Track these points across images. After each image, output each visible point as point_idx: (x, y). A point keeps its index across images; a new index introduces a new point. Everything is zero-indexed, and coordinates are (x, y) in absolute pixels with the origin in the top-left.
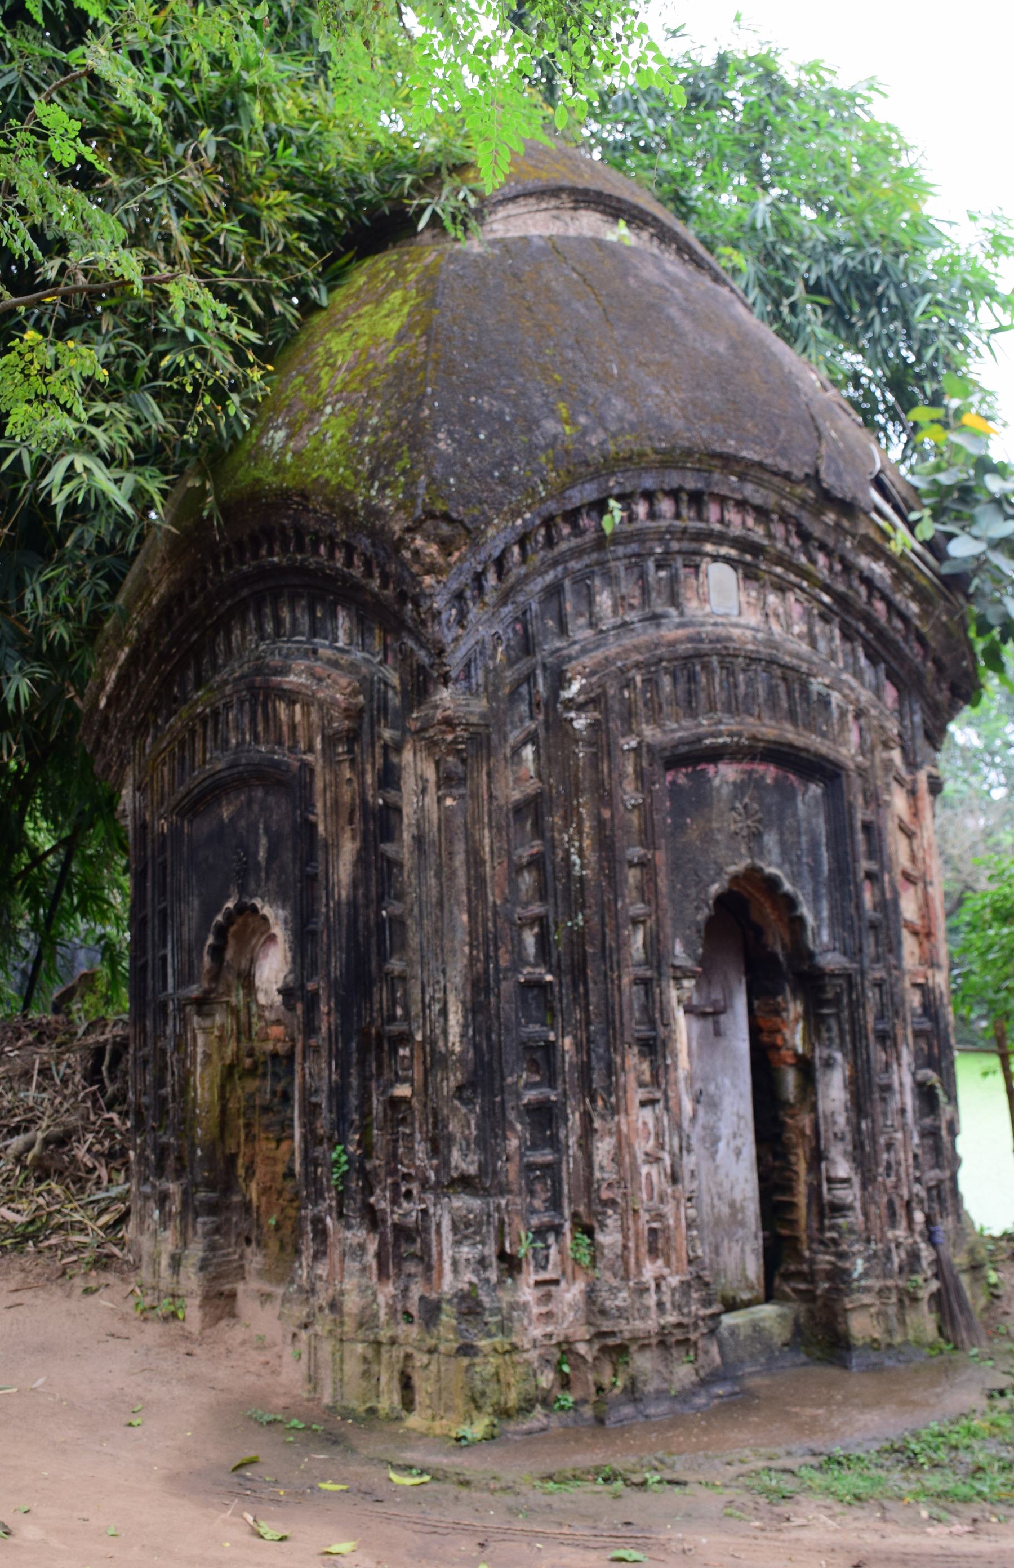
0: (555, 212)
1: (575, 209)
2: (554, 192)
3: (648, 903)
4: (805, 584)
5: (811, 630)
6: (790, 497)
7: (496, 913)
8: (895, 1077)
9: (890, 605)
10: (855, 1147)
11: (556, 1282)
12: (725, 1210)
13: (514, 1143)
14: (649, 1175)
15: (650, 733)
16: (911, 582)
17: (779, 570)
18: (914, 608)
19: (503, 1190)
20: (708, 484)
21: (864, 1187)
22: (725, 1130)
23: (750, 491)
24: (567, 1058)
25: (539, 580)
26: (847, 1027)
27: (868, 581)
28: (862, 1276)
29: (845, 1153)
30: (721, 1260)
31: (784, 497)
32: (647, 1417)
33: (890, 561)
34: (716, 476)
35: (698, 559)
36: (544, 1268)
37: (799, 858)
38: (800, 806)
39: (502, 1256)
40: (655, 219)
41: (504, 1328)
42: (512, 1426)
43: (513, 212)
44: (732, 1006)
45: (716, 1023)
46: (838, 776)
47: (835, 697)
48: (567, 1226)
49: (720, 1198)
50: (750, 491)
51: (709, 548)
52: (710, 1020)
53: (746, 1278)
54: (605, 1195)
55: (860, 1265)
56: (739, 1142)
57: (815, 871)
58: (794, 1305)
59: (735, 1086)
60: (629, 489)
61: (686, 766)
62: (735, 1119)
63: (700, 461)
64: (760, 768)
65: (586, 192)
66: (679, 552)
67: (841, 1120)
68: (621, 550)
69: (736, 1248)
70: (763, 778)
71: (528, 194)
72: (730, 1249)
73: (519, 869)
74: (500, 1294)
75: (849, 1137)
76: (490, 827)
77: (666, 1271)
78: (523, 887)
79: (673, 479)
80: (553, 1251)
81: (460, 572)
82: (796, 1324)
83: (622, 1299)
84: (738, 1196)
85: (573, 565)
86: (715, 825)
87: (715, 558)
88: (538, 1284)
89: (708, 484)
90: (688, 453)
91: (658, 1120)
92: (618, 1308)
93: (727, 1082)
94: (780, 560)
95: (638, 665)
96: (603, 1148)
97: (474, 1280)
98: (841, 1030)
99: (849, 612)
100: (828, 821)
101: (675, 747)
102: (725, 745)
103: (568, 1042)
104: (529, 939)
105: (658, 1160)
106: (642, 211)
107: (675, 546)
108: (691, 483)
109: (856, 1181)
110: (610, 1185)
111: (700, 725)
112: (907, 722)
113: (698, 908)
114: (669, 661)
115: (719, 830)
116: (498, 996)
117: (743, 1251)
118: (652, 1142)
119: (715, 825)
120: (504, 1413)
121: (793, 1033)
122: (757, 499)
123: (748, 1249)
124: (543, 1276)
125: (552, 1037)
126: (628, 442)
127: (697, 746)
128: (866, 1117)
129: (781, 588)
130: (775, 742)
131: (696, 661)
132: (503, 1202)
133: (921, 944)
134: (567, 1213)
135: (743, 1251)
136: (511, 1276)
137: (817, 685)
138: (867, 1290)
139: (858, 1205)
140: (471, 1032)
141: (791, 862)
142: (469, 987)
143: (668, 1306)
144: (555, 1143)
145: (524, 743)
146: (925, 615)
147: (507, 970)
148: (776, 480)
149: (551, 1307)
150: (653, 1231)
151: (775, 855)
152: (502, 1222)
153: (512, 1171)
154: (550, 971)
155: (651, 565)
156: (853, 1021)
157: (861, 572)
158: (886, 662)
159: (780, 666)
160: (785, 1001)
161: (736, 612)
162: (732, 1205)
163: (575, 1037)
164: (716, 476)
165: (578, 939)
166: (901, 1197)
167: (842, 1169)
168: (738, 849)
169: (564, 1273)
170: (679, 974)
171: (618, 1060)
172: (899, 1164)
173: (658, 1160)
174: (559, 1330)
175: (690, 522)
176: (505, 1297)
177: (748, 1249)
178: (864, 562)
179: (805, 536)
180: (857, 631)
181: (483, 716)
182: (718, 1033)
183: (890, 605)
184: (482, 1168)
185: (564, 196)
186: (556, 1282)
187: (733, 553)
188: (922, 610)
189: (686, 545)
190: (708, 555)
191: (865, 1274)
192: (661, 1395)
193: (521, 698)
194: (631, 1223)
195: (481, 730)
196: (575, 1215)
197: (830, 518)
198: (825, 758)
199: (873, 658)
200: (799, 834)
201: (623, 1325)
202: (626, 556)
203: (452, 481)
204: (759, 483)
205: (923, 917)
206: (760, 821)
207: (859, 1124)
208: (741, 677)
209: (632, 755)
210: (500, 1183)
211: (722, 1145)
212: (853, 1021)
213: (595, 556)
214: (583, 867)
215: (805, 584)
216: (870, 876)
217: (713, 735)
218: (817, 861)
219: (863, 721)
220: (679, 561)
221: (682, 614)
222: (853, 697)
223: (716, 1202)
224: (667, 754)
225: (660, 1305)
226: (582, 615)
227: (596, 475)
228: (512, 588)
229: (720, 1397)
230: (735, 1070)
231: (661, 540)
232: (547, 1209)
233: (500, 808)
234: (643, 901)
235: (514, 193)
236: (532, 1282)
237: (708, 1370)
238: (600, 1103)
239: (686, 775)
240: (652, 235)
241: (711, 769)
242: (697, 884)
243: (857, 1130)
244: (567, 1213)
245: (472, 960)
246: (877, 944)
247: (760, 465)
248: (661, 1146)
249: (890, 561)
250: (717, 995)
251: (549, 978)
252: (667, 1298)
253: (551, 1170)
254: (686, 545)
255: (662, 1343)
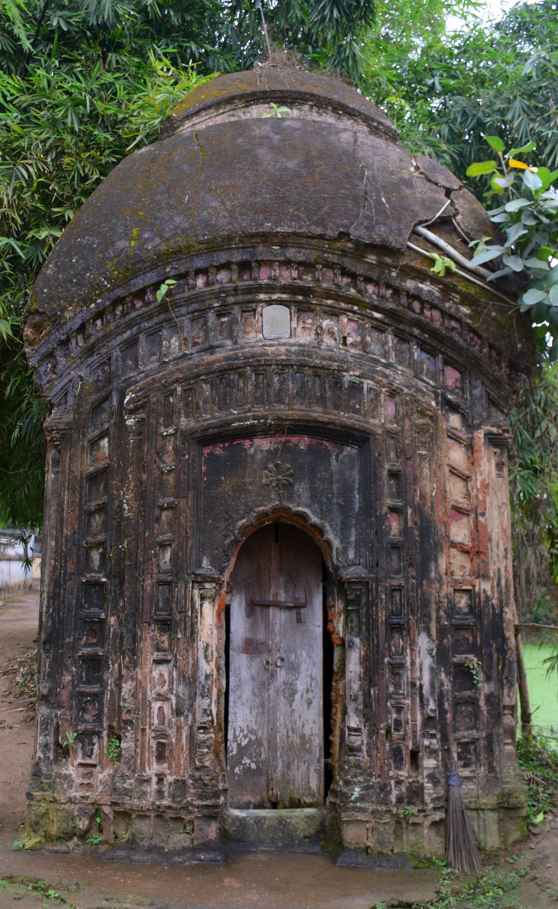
0: (231, 113)
1: (247, 106)
2: (229, 100)
3: (174, 533)
4: (356, 308)
5: (363, 339)
6: (331, 250)
7: (67, 541)
8: (408, 659)
9: (443, 313)
10: (365, 706)
11: (94, 766)
12: (297, 740)
13: (67, 678)
14: (160, 708)
15: (184, 423)
16: (457, 293)
17: (329, 302)
18: (465, 310)
19: (60, 707)
20: (253, 256)
21: (370, 736)
22: (301, 686)
23: (291, 253)
24: (112, 630)
25: (120, 337)
26: (364, 620)
27: (415, 296)
28: (357, 801)
29: (356, 710)
30: (291, 773)
31: (326, 252)
32: (131, 861)
33: (434, 279)
34: (260, 248)
35: (254, 305)
36: (90, 756)
37: (329, 500)
38: (334, 462)
39: (57, 744)
40: (312, 95)
41: (51, 787)
42: (49, 846)
43: (195, 122)
44: (311, 603)
45: (299, 614)
46: (368, 439)
47: (367, 383)
48: (105, 733)
49: (293, 731)
50: (291, 253)
51: (262, 296)
52: (294, 611)
53: (310, 788)
54: (125, 717)
55: (357, 791)
56: (311, 695)
57: (345, 509)
58: (325, 812)
59: (309, 656)
60: (183, 270)
61: (221, 442)
62: (309, 679)
63: (241, 241)
64: (294, 440)
65: (254, 94)
66: (235, 303)
67: (356, 686)
68: (183, 310)
69: (303, 768)
70: (297, 445)
71: (204, 109)
72: (298, 767)
73: (91, 514)
74: (54, 767)
75: (361, 699)
76: (68, 489)
77: (168, 772)
78: (95, 525)
79: (223, 257)
80: (96, 747)
81: (47, 342)
82: (322, 824)
83: (129, 783)
84: (307, 732)
85: (146, 324)
86: (247, 480)
87: (270, 302)
88: (81, 765)
89: (253, 256)
90: (229, 239)
91: (170, 673)
92: (125, 789)
93: (304, 654)
94: (328, 295)
95: (177, 381)
96: (127, 687)
97: (42, 756)
98: (360, 622)
99: (401, 322)
100: (360, 472)
101: (206, 429)
102: (253, 425)
103: (112, 620)
104: (96, 556)
105: (167, 699)
106: (301, 93)
107: (231, 300)
108: (237, 257)
109: (365, 731)
110: (129, 711)
111: (231, 414)
112: (467, 395)
113: (226, 536)
114: (206, 374)
115: (250, 483)
116: (65, 590)
117: (308, 769)
118: (166, 687)
119: (247, 480)
120: (48, 838)
121: (338, 623)
122: (300, 257)
123: (312, 769)
124: (88, 761)
125: (103, 616)
126: (181, 241)
127: (227, 428)
128: (374, 686)
129: (334, 313)
130: (299, 420)
131: (232, 372)
132: (59, 713)
133: (472, 560)
134: (105, 725)
135: (308, 769)
136: (65, 758)
137: (348, 377)
138: (363, 810)
139: (364, 748)
140: (51, 610)
141: (321, 504)
142: (52, 584)
143: (166, 794)
144: (101, 681)
145: (101, 437)
146: (475, 315)
147: (72, 574)
148: (314, 242)
149: (91, 781)
150: (160, 745)
151: (305, 497)
152: (58, 726)
153: (65, 695)
154: (105, 576)
155: (211, 316)
156: (368, 616)
157: (408, 292)
158: (443, 353)
159: (310, 367)
160: (334, 601)
161: (288, 335)
162: (302, 737)
163: (118, 617)
164: (260, 248)
165: (121, 557)
166: (407, 747)
167: (354, 721)
168: (269, 496)
169: (100, 762)
170: (199, 579)
171: (139, 633)
172: (407, 723)
173: (167, 699)
174: (92, 796)
175: (246, 282)
176: (56, 769)
177: (312, 769)
178: (410, 284)
179: (353, 276)
180: (411, 334)
181: (68, 424)
182: (299, 621)
183: (443, 313)
184: (50, 691)
185: (236, 101)
186: (94, 766)
187: (284, 296)
188: (473, 311)
189: (241, 298)
190: (261, 301)
191: (362, 798)
192: (150, 850)
193: (104, 410)
194: (139, 736)
195: (67, 432)
196: (111, 727)
197: (372, 258)
198: (351, 428)
199: (431, 351)
200: (331, 483)
201: (127, 800)
202: (188, 313)
203: (45, 290)
204: (300, 246)
205: (473, 540)
206: (291, 476)
207: (370, 690)
208: (276, 379)
209: (172, 438)
210: (59, 702)
211: (297, 696)
212: (368, 616)
213: (162, 316)
214: (129, 511)
215: (356, 308)
216: (393, 510)
217: (239, 420)
218: (349, 501)
219: (397, 399)
220: (237, 310)
221: (236, 343)
222: (385, 381)
223: (290, 733)
224: (198, 435)
225: (160, 793)
226: (154, 355)
227: (154, 266)
228: (93, 345)
229: (202, 860)
230: (311, 646)
231: (218, 298)
232: (94, 721)
233: (75, 477)
234: (171, 532)
235: (196, 110)
236: (76, 763)
237: (200, 841)
238: (127, 659)
239: (223, 448)
240: (312, 106)
241: (247, 443)
242: (226, 520)
243: (367, 695)
244: (105, 725)
245: (55, 567)
246: (399, 559)
247: (294, 234)
248: (171, 690)
249: (434, 279)
250: (301, 595)
251: (104, 580)
252: (165, 789)
253: (97, 697)
254: (241, 298)
255: (159, 816)
